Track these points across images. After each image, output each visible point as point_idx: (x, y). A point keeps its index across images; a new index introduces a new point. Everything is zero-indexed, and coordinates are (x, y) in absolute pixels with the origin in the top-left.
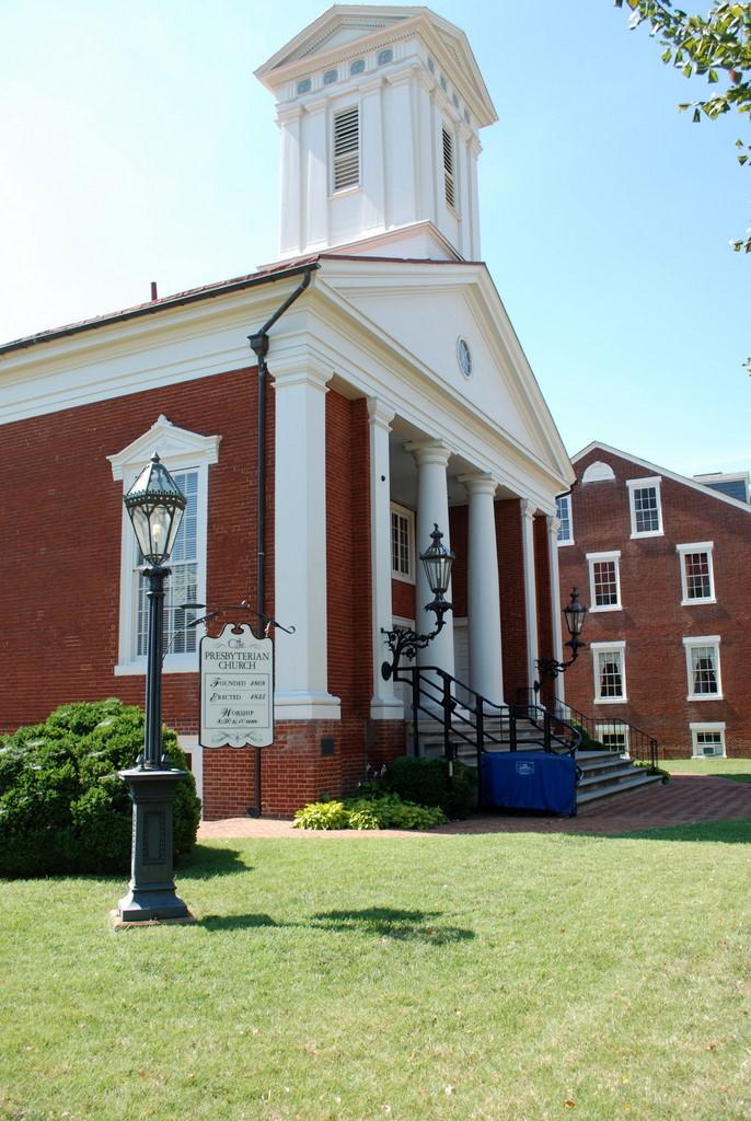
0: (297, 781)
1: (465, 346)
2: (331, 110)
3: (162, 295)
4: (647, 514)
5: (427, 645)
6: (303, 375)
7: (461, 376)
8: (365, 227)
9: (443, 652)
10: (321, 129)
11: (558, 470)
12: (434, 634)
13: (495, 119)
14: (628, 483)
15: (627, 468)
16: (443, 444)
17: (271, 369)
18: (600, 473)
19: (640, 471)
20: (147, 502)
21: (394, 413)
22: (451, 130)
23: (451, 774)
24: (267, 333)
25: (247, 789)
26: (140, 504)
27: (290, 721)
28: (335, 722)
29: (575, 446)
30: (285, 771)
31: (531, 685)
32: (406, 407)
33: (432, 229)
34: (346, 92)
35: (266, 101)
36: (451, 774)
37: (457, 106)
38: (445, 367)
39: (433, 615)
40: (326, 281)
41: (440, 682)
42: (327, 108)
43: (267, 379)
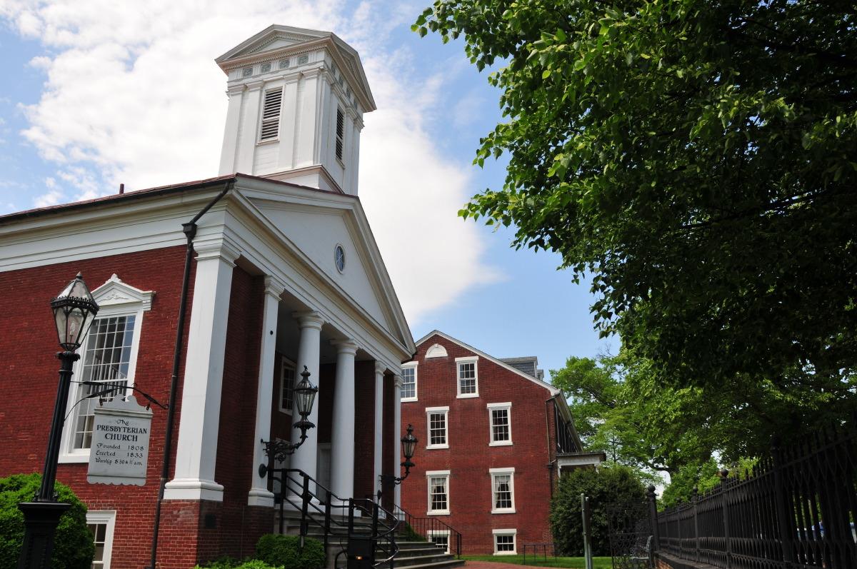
0: (185, 546)
1: (341, 250)
2: (264, 90)
3: (126, 191)
4: (468, 382)
5: (293, 452)
6: (218, 254)
7: (335, 268)
8: (272, 162)
9: (307, 457)
10: (255, 101)
11: (405, 345)
12: (299, 444)
13: (374, 108)
14: (457, 359)
15: (456, 350)
16: (319, 315)
17: (196, 246)
18: (437, 352)
19: (465, 352)
20: (67, 305)
21: (239, 253)
22: (343, 109)
23: (302, 546)
24: (196, 223)
25: (146, 553)
26: (62, 307)
27: (183, 500)
28: (218, 503)
29: (418, 334)
30: (176, 538)
31: (376, 493)
32: (392, 365)
33: (323, 172)
34: (275, 77)
35: (221, 79)
36: (302, 546)
37: (349, 96)
38: (326, 265)
39: (299, 432)
40: (242, 192)
41: (301, 480)
42: (262, 88)
43: (193, 253)
